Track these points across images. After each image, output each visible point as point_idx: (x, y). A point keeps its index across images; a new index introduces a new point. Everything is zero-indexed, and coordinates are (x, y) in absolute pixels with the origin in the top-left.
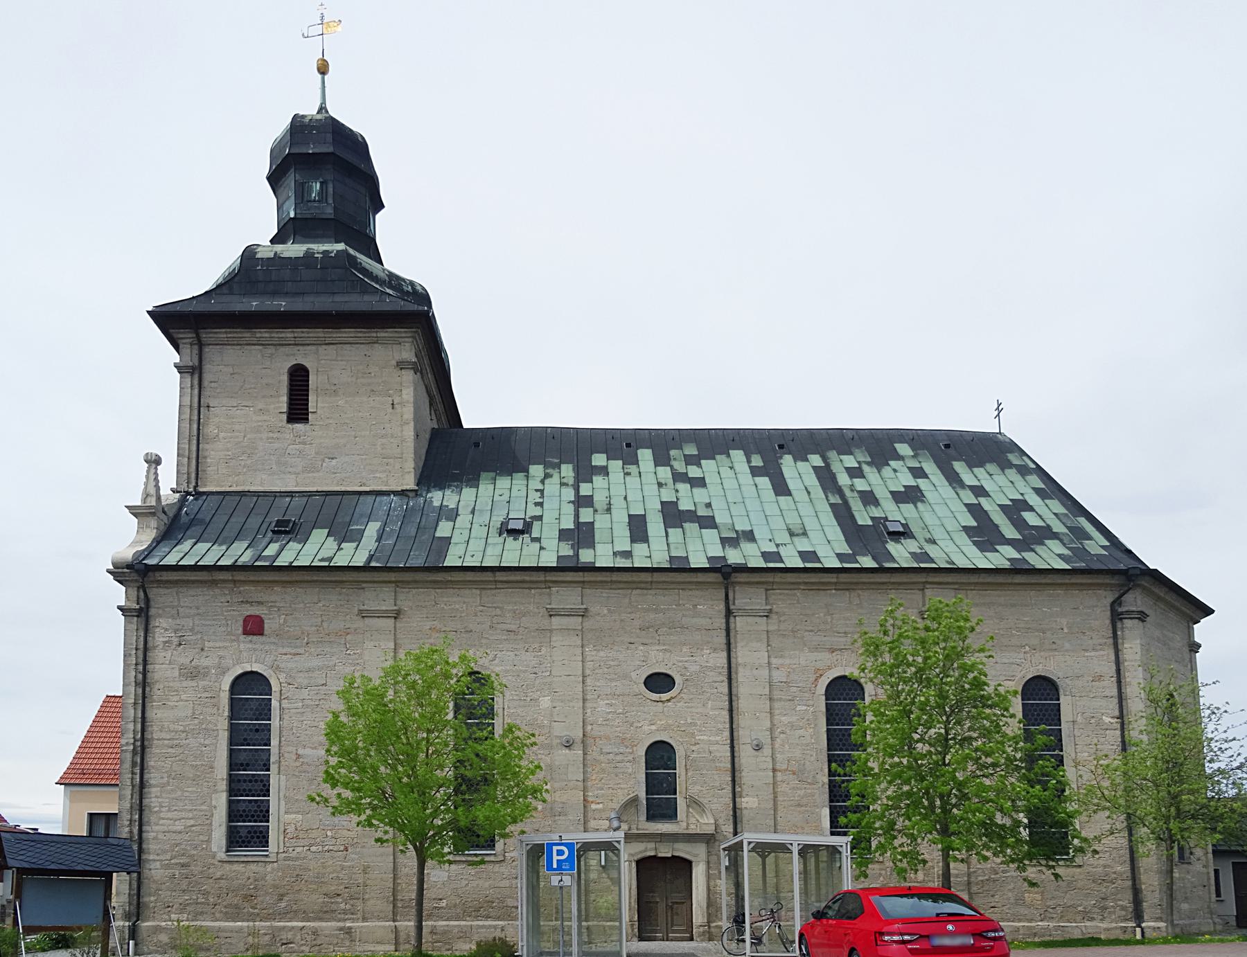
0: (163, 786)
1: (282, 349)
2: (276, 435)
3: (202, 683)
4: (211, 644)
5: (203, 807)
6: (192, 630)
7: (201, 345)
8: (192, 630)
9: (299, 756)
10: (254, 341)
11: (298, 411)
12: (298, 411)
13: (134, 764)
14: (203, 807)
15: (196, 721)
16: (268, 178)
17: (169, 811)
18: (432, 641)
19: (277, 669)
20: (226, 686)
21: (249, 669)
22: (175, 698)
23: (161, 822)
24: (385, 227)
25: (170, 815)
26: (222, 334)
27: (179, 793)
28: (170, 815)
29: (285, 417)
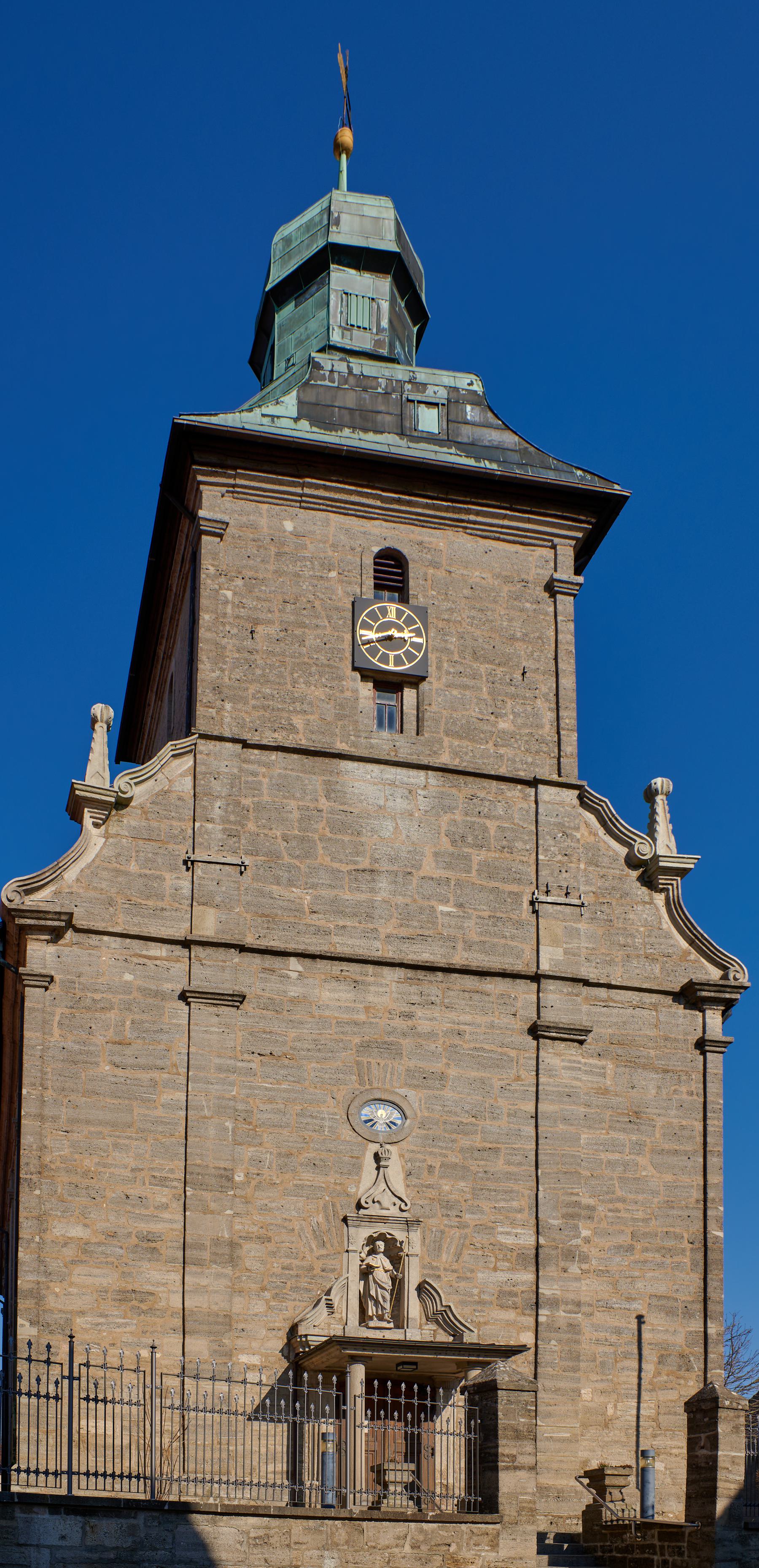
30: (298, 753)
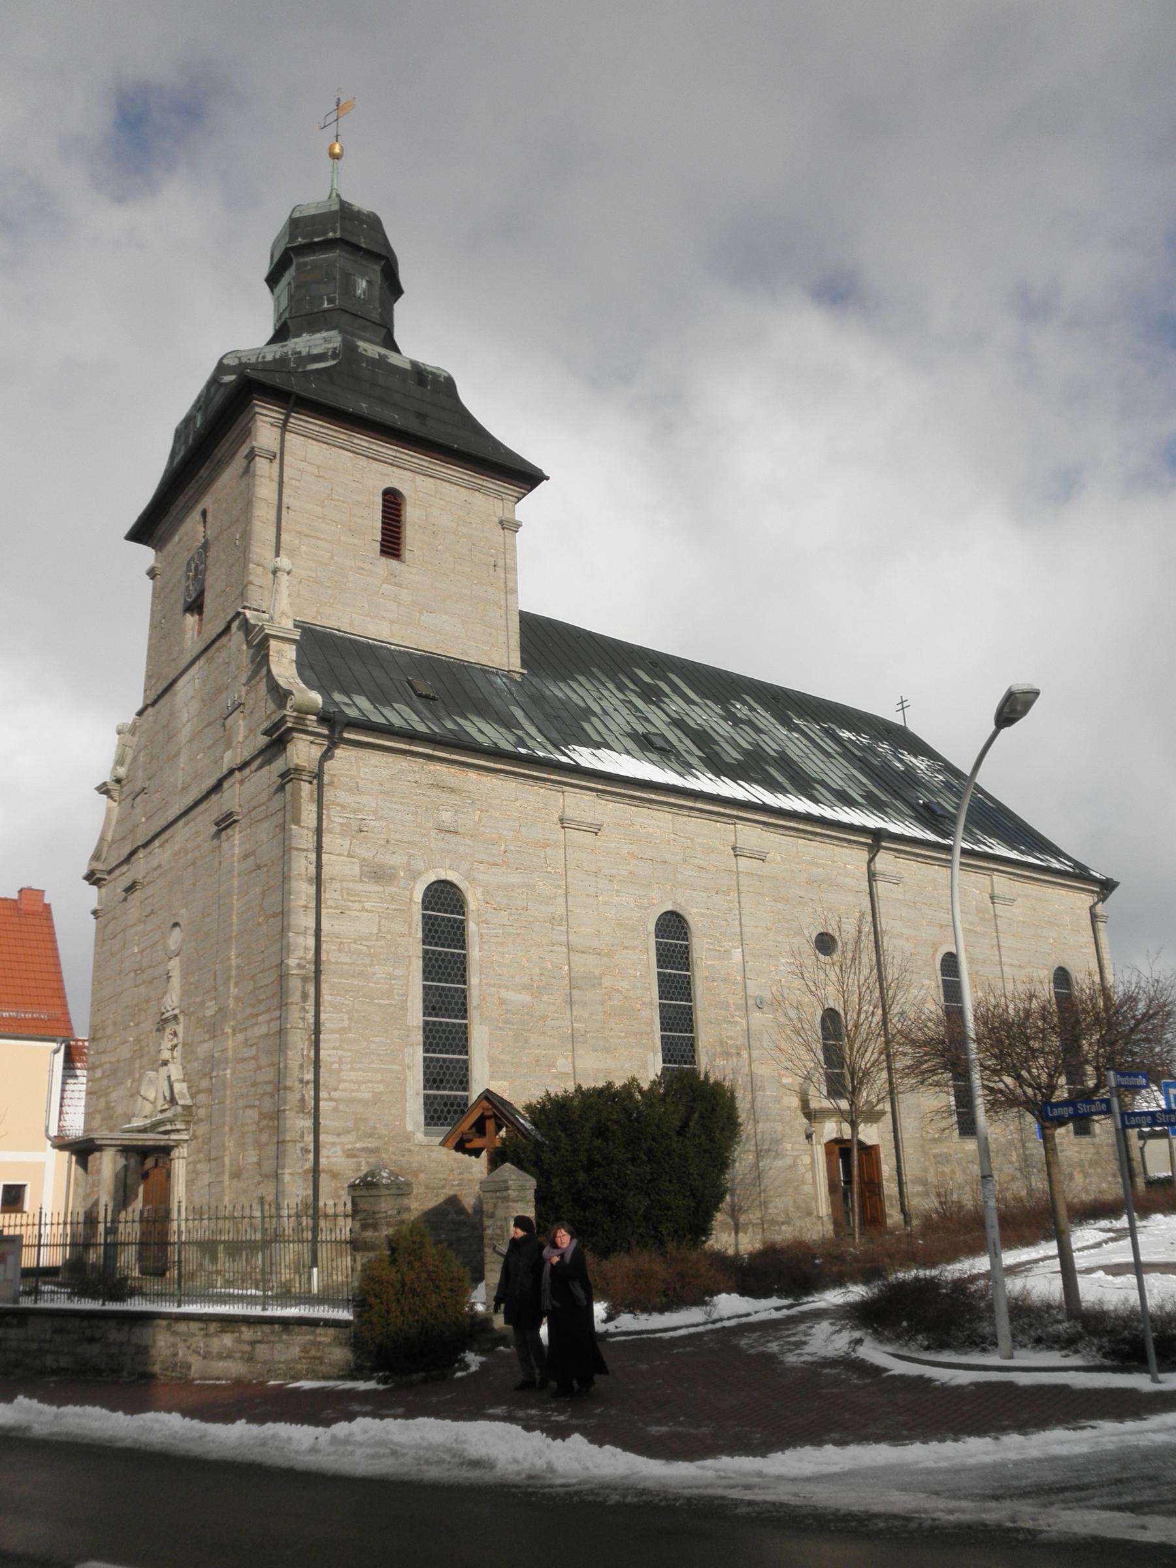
0: (342, 1031)
1: (376, 465)
2: (367, 567)
3: (390, 889)
4: (398, 837)
5: (396, 1067)
6: (375, 812)
7: (284, 428)
8: (375, 812)
9: (503, 1002)
10: (348, 445)
11: (392, 543)
12: (392, 543)
13: (305, 997)
14: (396, 1067)
15: (383, 943)
16: (295, 224)
17: (352, 1069)
18: (631, 868)
19: (473, 881)
20: (418, 897)
21: (443, 878)
22: (357, 906)
23: (379, 1077)
24: (403, 314)
25: (354, 1075)
26: (315, 425)
27: (364, 1044)
28: (354, 1075)
29: (378, 546)
30: (384, 530)
